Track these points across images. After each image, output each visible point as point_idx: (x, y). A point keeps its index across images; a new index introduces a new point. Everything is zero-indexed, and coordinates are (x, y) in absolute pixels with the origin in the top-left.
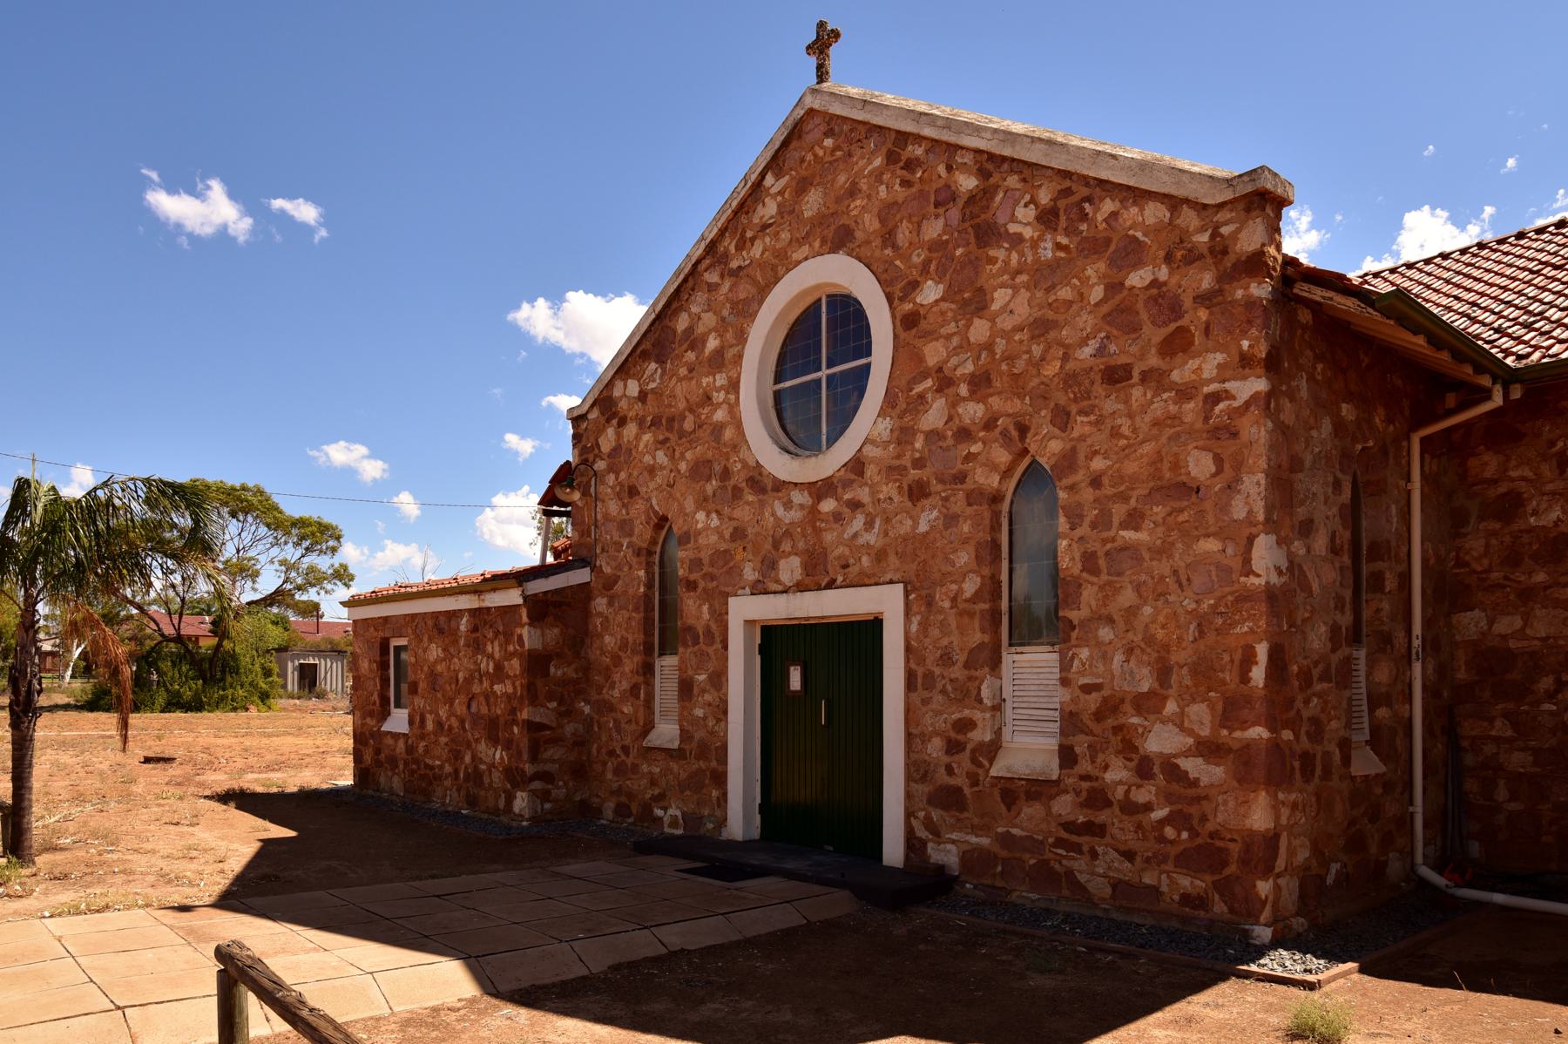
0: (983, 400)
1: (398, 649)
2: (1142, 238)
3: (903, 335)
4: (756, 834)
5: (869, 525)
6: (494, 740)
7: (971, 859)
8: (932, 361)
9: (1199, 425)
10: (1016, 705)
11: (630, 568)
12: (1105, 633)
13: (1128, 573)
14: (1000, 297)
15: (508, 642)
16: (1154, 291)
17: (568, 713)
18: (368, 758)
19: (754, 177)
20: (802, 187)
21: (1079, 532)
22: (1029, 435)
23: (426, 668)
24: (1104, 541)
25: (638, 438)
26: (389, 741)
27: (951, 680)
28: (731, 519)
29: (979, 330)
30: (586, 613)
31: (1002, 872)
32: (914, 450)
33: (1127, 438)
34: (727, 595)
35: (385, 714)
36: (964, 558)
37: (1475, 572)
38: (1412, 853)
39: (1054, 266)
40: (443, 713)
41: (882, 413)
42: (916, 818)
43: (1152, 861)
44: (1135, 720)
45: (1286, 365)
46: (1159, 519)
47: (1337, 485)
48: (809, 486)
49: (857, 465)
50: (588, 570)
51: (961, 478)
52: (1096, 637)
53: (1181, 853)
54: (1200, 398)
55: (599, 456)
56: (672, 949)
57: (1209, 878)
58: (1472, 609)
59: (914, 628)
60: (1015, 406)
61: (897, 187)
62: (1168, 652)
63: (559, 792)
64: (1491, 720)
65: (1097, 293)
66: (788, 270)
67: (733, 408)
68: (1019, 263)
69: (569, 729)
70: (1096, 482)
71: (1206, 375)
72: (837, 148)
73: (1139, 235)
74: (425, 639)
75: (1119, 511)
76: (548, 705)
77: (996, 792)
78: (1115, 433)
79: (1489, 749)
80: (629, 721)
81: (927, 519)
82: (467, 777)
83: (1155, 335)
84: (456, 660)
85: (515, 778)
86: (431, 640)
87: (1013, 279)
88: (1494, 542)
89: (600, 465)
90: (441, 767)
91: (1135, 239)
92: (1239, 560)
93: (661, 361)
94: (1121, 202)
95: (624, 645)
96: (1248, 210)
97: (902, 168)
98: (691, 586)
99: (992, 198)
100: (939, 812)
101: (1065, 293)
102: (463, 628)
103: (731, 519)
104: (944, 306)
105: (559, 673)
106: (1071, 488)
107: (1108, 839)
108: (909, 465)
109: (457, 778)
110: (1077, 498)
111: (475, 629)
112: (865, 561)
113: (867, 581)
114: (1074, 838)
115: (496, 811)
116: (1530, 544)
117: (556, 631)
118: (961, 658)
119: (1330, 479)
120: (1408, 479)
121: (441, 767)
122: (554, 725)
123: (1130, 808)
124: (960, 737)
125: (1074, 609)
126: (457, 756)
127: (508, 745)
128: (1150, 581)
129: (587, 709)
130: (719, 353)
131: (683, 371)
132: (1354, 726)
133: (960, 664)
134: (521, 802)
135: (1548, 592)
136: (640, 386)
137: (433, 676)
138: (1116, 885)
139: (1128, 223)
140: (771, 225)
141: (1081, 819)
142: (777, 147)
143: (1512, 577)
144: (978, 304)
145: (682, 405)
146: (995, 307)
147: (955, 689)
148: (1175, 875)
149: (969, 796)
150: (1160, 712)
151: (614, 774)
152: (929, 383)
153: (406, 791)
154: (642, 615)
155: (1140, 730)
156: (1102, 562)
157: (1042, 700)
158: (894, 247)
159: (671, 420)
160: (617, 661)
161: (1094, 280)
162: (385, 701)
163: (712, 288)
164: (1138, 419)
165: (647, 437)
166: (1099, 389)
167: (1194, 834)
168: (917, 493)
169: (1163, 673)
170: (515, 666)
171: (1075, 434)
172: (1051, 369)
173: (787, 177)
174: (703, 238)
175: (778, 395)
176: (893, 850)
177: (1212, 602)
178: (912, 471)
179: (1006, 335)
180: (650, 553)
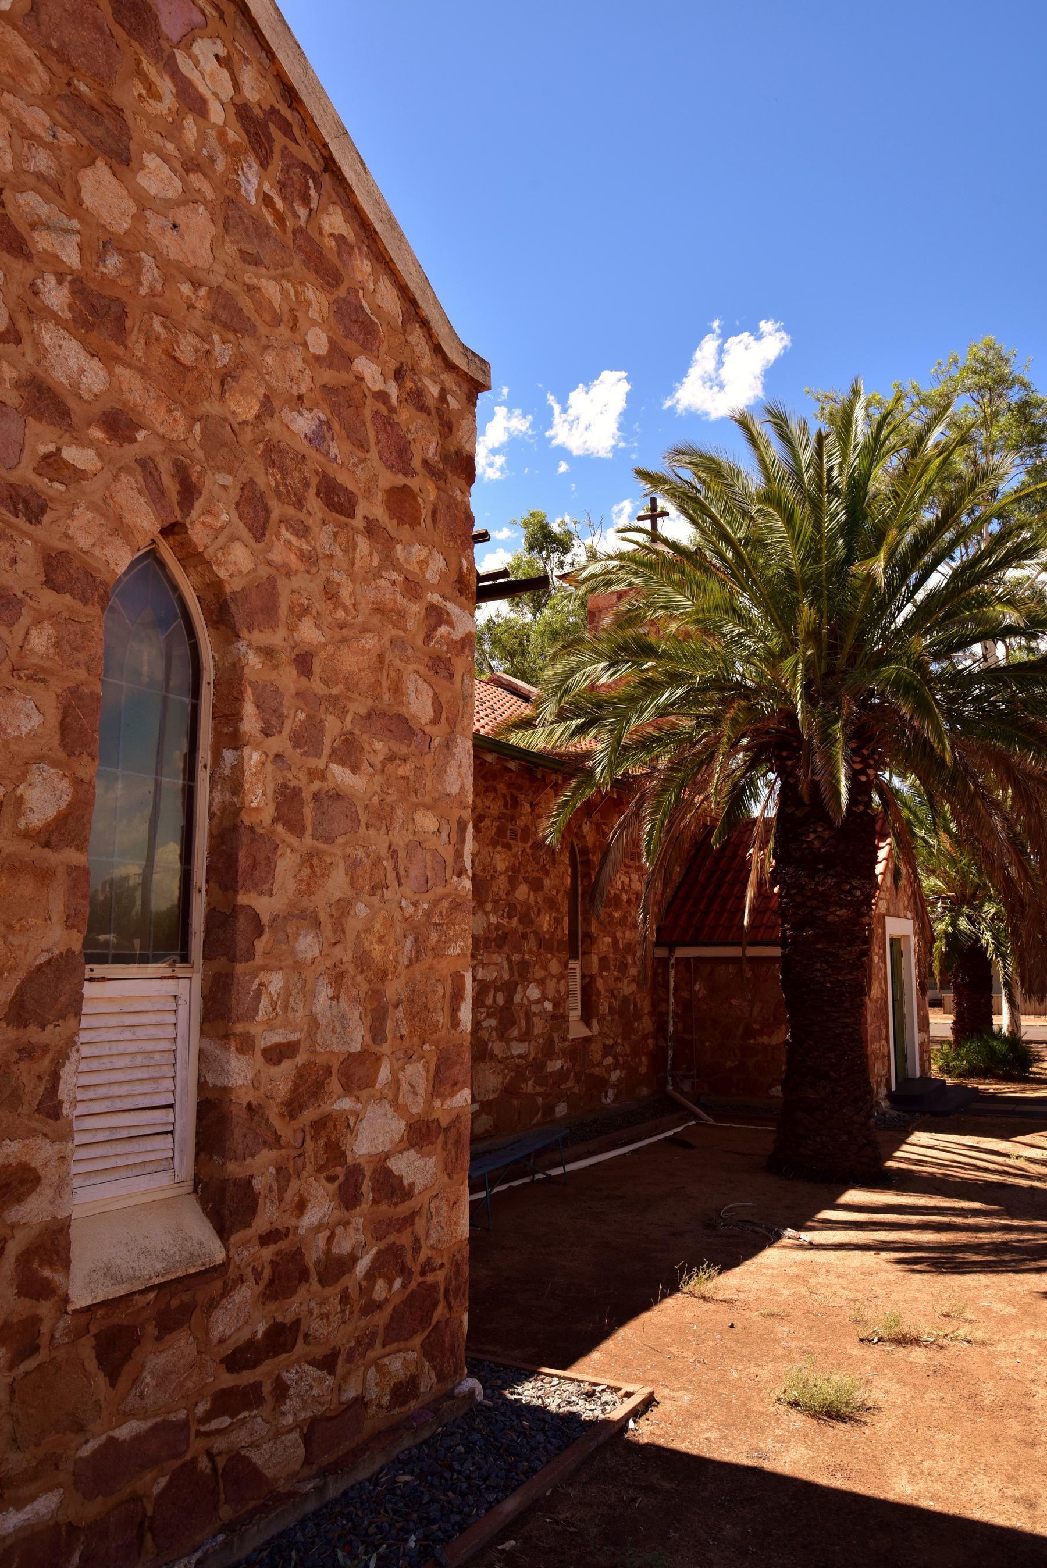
10: (166, 1116)
12: (307, 945)
13: (340, 840)
44: (346, 1104)
52: (293, 951)
53: (392, 1317)
75: (332, 727)
77: (87, 1350)
92: (451, 849)
106: (268, 653)
110: (273, 676)
125: (261, 893)
157: (140, 1088)
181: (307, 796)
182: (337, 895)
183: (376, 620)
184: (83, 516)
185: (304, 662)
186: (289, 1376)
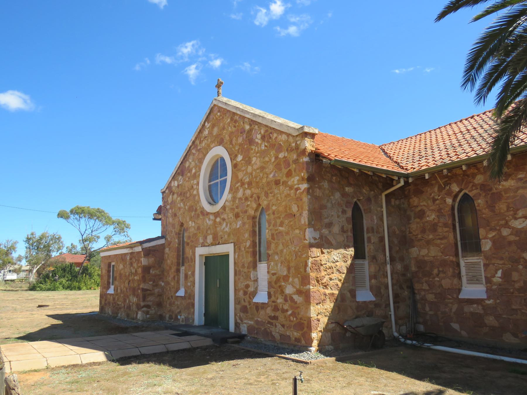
0: (250, 189)
1: (113, 266)
2: (282, 144)
3: (234, 170)
4: (203, 323)
5: (227, 225)
6: (134, 295)
7: (250, 329)
8: (240, 178)
9: (294, 197)
11: (174, 239)
12: (276, 257)
13: (281, 239)
14: (254, 159)
15: (138, 263)
16: (284, 159)
17: (156, 285)
18: (103, 303)
19: (202, 123)
20: (213, 126)
21: (270, 228)
22: (260, 199)
23: (119, 272)
24: (276, 230)
25: (177, 199)
27: (244, 272)
28: (197, 223)
29: (250, 169)
30: (163, 253)
31: (257, 333)
32: (236, 203)
33: (280, 200)
34: (196, 247)
35: (108, 288)
36: (247, 235)
37: (414, 235)
38: (391, 328)
39: (264, 151)
40: (122, 286)
41: (229, 193)
42: (237, 316)
43: (289, 327)
44: (283, 284)
45: (317, 179)
46: (287, 223)
47: (344, 212)
48: (214, 214)
49: (224, 208)
51: (246, 212)
54: (294, 189)
55: (168, 204)
56: (142, 353)
57: (301, 332)
58: (414, 247)
59: (236, 257)
60: (257, 191)
61: (233, 128)
62: (289, 263)
63: (152, 311)
64: (422, 283)
65: (273, 159)
66: (210, 150)
67: (198, 190)
68: (258, 150)
69: (156, 290)
70: (274, 213)
71: (295, 183)
72: (220, 116)
73: (282, 143)
74: (119, 262)
75: (278, 221)
76: (149, 283)
78: (277, 200)
79: (423, 293)
80: (173, 288)
81: (239, 223)
82: (127, 307)
83: (285, 171)
84: (126, 269)
85: (139, 307)
86: (120, 263)
87: (256, 155)
88: (418, 225)
89: (168, 207)
90: (121, 304)
91: (281, 144)
93: (182, 175)
94: (278, 134)
95: (172, 264)
96: (302, 137)
97: (234, 122)
98: (188, 244)
99: (252, 132)
100: (243, 314)
101: (267, 159)
102: (128, 259)
103: (197, 223)
104: (243, 162)
105: (154, 272)
106: (268, 215)
107: (279, 321)
108: (235, 208)
109: (124, 308)
111: (131, 259)
112: (226, 236)
113: (226, 242)
114: (272, 321)
115: (133, 319)
116: (428, 226)
117: (153, 259)
118: (246, 265)
119: (340, 210)
120: (382, 207)
121: (121, 304)
122: (151, 289)
123: (284, 311)
124: (246, 290)
126: (125, 301)
128: (285, 242)
129: (163, 284)
130: (195, 173)
131: (187, 179)
132: (356, 286)
133: (246, 267)
135: (434, 241)
136: (178, 183)
137: (121, 275)
138: (281, 335)
139: (279, 140)
140: (207, 137)
141: (273, 315)
142: (207, 115)
143: (424, 236)
145: (187, 189)
146: (253, 162)
147: (245, 275)
148: (293, 332)
149: (248, 308)
150: (288, 281)
151: (169, 305)
152: (239, 184)
153: (112, 313)
154: (176, 253)
155: (284, 287)
156: (275, 236)
158: (232, 145)
160: (170, 268)
161: (272, 156)
162: (109, 283)
163: (194, 154)
164: (282, 195)
165: (179, 199)
166: (274, 186)
167: (297, 319)
168: (237, 216)
169: (289, 269)
170: (140, 271)
171: (269, 199)
172: (264, 181)
173: (210, 123)
174: (191, 140)
175: (210, 186)
176: (232, 328)
177: (298, 248)
178: (236, 210)
179: (255, 170)
180: (179, 234)
186: (277, 324)
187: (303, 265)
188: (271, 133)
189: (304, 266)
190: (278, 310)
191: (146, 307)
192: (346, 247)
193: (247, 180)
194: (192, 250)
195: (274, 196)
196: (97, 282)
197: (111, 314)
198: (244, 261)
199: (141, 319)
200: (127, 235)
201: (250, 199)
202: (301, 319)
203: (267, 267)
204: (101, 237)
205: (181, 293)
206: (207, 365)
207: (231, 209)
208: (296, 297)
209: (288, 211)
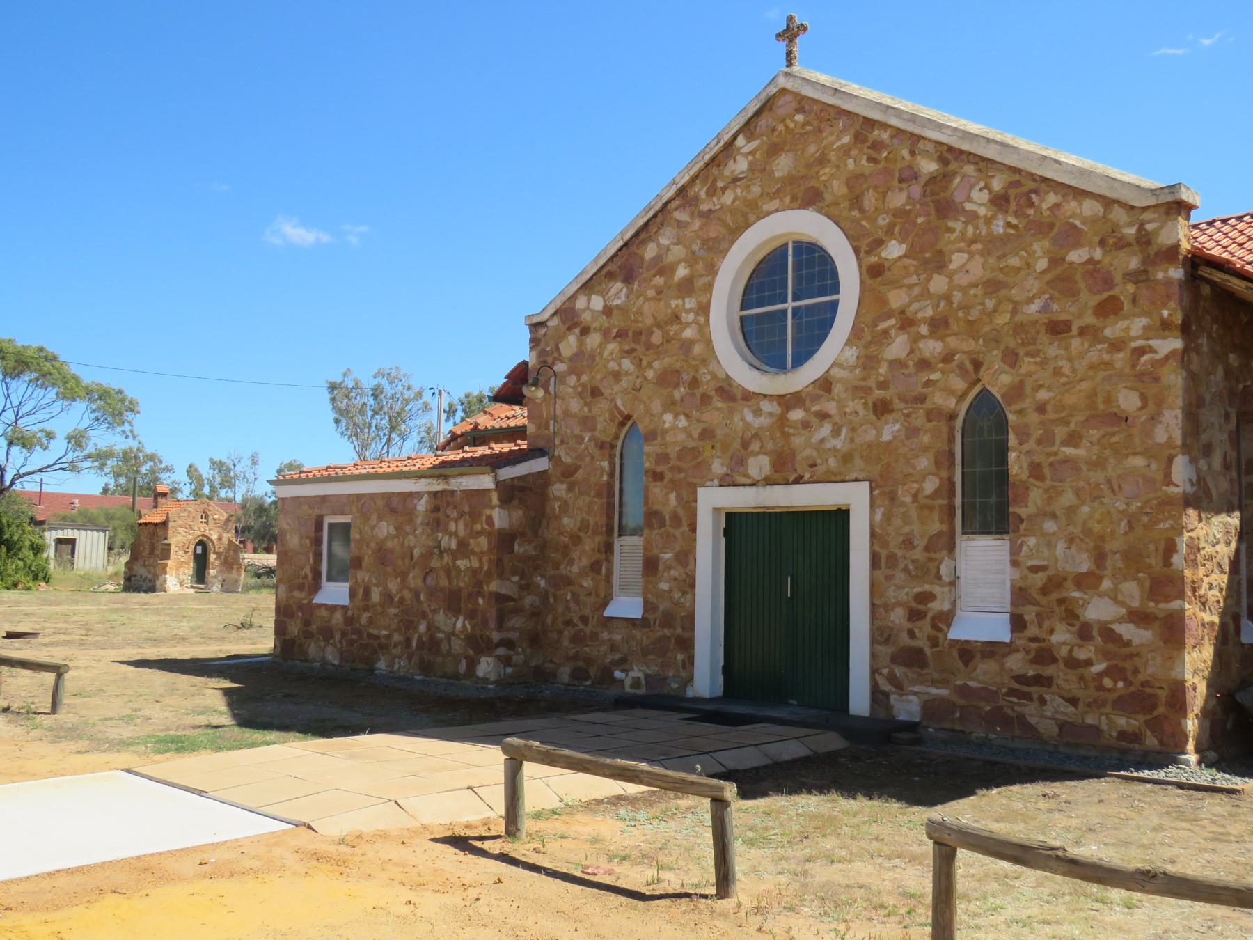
9: (1127, 370)
11: (593, 458)
12: (1050, 526)
15: (474, 521)
16: (1090, 267)
17: (527, 587)
18: (294, 629)
20: (774, 150)
26: (324, 613)
27: (913, 561)
30: (543, 497)
33: (1067, 376)
35: (316, 587)
36: (924, 463)
39: (1004, 240)
41: (849, 343)
43: (1097, 704)
44: (1076, 594)
45: (1194, 328)
46: (1095, 439)
49: (825, 384)
50: (545, 459)
54: (1128, 351)
59: (878, 517)
60: (970, 345)
63: (518, 659)
65: (1042, 264)
67: (704, 328)
78: (1057, 372)
86: (380, 518)
89: (560, 367)
91: (1075, 226)
99: (951, 181)
100: (903, 669)
101: (1014, 261)
103: (699, 421)
104: (907, 261)
105: (522, 550)
108: (874, 386)
114: (1025, 689)
117: (520, 512)
121: (389, 637)
122: (516, 596)
127: (471, 615)
129: (543, 583)
131: (651, 293)
134: (486, 667)
144: (939, 263)
146: (953, 266)
152: (892, 322)
158: (861, 210)
159: (638, 334)
160: (576, 540)
162: (317, 574)
163: (680, 224)
167: (1128, 683)
168: (882, 409)
169: (1100, 557)
170: (483, 542)
172: (1003, 319)
174: (674, 182)
176: (859, 702)
177: (1139, 504)
178: (877, 391)
179: (964, 290)
180: (613, 447)
181: (1045, 464)
182: (1068, 504)
183: (1091, 373)
184: (938, 394)
185: (1041, 409)
186: (1048, 697)
187: (1157, 550)
188: (1036, 192)
189: (1161, 551)
190: (1054, 660)
191: (504, 646)
192: (1229, 510)
193: (929, 312)
194: (678, 495)
195: (1043, 364)
196: (33, 569)
197: (336, 662)
198: (913, 531)
199: (493, 678)
200: (132, 432)
201: (940, 365)
202: (1144, 684)
203: (95, 533)
204: (58, 435)
205: (626, 605)
206: (972, 798)
207: (856, 389)
208: (1126, 631)
209: (1101, 407)
